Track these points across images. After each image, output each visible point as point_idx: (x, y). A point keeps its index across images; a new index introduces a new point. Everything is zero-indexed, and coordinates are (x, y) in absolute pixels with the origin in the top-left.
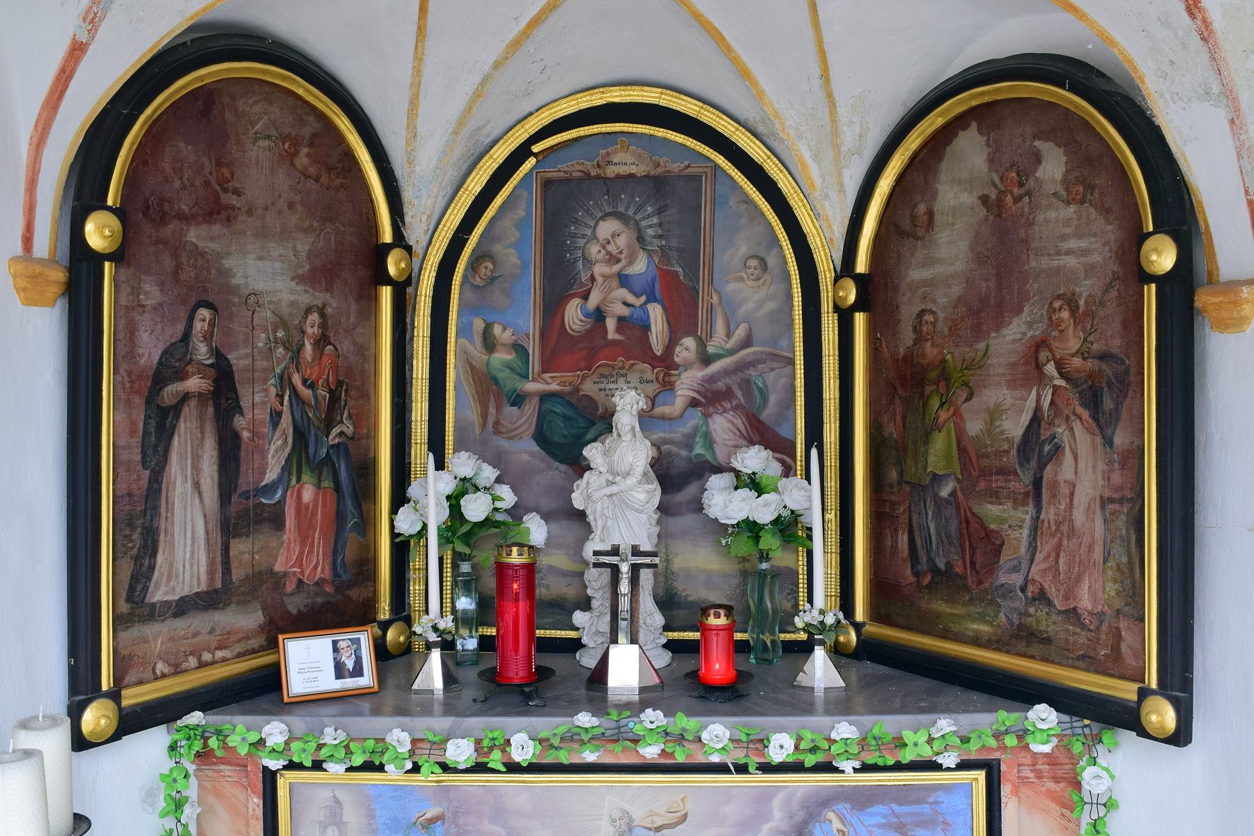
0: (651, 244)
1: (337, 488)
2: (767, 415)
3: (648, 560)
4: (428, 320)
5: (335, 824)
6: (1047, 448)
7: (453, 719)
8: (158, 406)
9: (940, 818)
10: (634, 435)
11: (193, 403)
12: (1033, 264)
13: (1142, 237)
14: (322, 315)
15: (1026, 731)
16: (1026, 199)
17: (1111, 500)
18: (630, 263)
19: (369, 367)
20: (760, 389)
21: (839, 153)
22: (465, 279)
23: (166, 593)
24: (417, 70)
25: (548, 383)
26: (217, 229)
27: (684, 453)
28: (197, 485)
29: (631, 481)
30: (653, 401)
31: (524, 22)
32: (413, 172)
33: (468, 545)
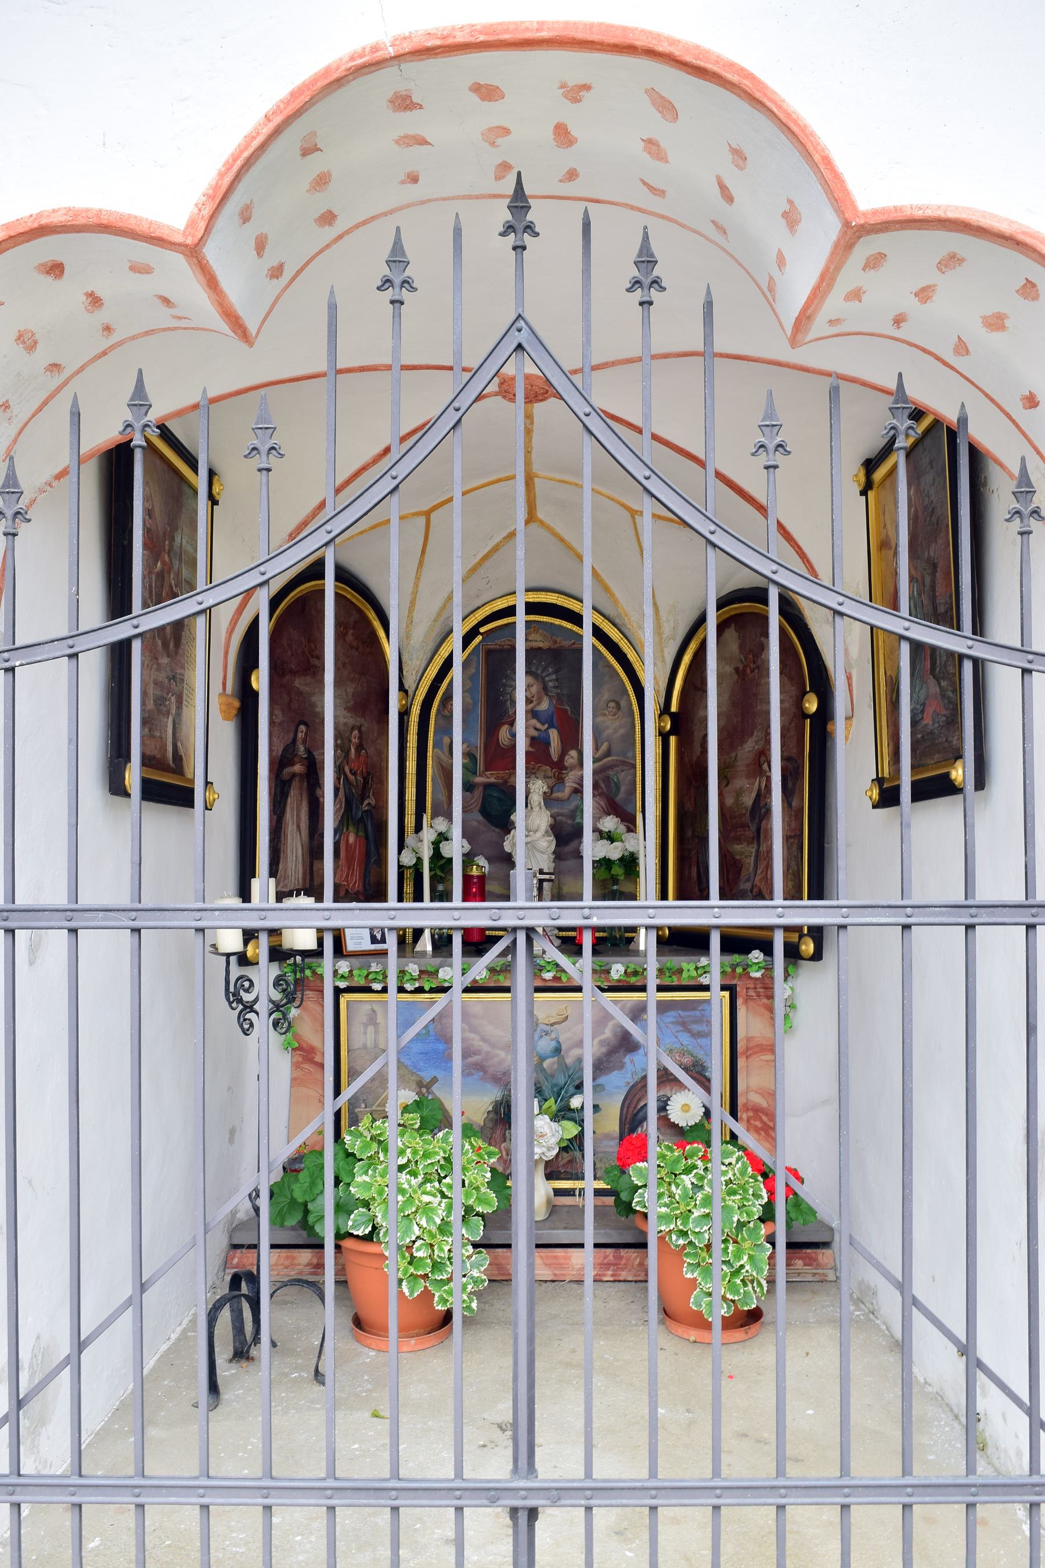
0: (551, 692)
1: (367, 837)
2: (620, 797)
3: (547, 877)
4: (415, 737)
5: (372, 1024)
6: (763, 811)
7: (441, 959)
8: (281, 780)
9: (705, 1019)
10: (541, 808)
11: (297, 779)
12: (759, 708)
13: (805, 693)
14: (360, 731)
15: (748, 966)
16: (757, 671)
17: (791, 837)
18: (539, 703)
19: (384, 764)
20: (616, 784)
21: (661, 639)
22: (438, 711)
23: (283, 887)
24: (416, 585)
25: (488, 778)
26: (308, 679)
27: (570, 822)
28: (298, 827)
29: (539, 834)
30: (552, 789)
31: (480, 556)
32: (409, 644)
33: (442, 872)
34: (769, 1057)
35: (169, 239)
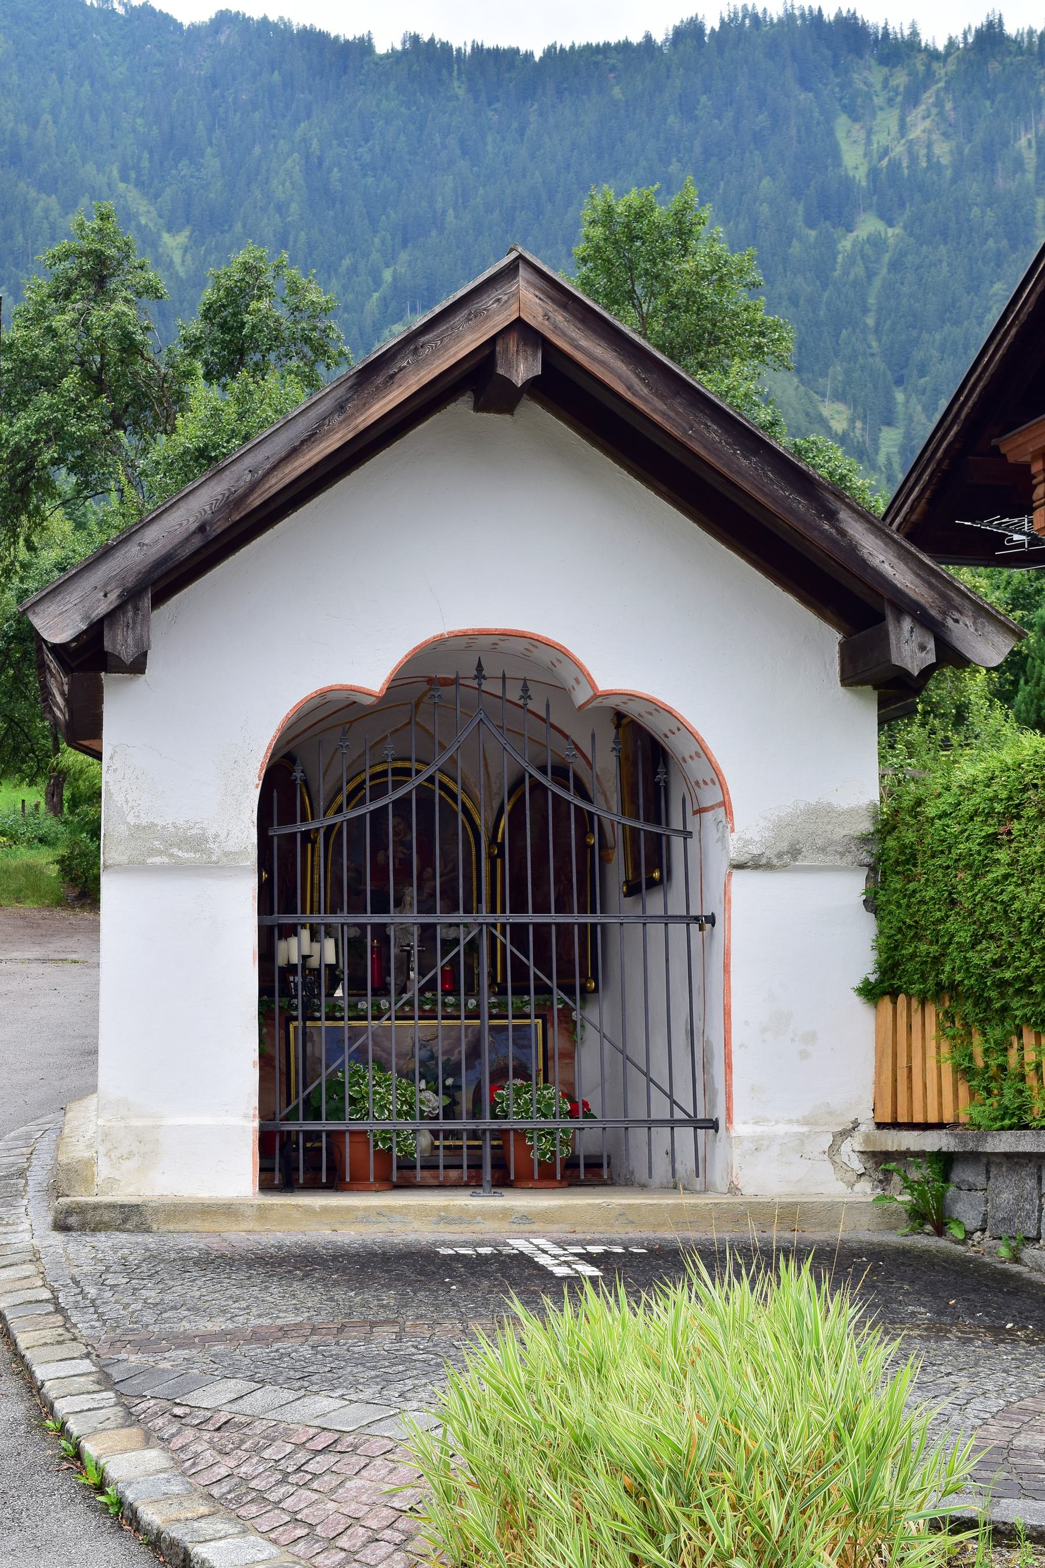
34: (568, 1061)
35: (176, 541)
